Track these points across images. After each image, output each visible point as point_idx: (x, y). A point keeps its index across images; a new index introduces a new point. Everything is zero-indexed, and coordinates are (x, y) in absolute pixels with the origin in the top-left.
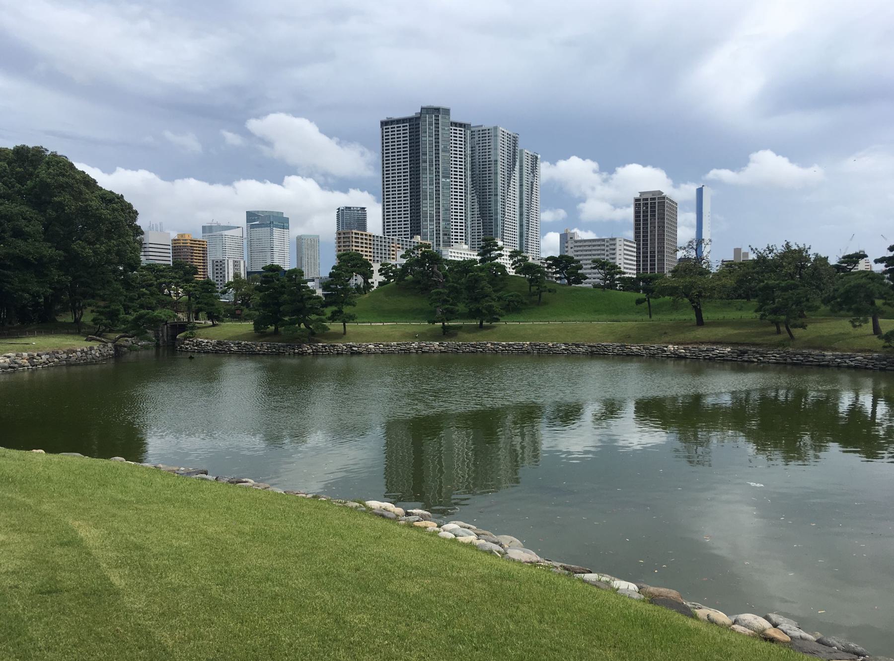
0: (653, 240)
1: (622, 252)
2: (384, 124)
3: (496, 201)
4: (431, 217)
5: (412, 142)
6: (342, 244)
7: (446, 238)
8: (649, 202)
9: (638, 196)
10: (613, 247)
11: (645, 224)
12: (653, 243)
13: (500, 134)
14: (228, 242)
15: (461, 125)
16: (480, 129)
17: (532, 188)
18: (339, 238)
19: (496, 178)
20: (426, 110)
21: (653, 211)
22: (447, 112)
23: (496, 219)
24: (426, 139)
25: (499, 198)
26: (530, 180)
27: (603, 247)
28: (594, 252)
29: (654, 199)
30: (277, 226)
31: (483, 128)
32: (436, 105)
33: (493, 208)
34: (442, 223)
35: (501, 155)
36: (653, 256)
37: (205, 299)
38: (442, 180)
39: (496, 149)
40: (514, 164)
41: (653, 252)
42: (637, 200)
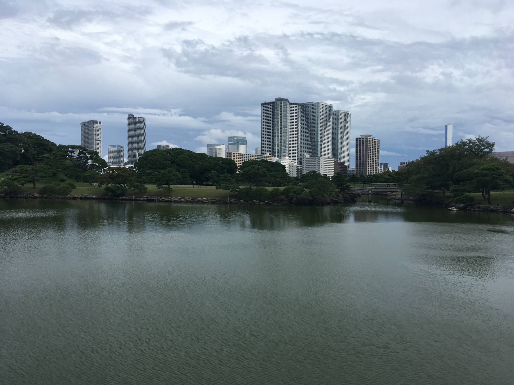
0: (363, 156)
1: (323, 168)
2: (263, 104)
3: (317, 136)
11: (360, 149)
13: (320, 105)
15: (296, 104)
19: (318, 126)
21: (363, 144)
22: (286, 100)
23: (317, 144)
25: (319, 135)
30: (241, 144)
38: (283, 129)
39: (318, 113)
40: (329, 119)
42: (357, 139)
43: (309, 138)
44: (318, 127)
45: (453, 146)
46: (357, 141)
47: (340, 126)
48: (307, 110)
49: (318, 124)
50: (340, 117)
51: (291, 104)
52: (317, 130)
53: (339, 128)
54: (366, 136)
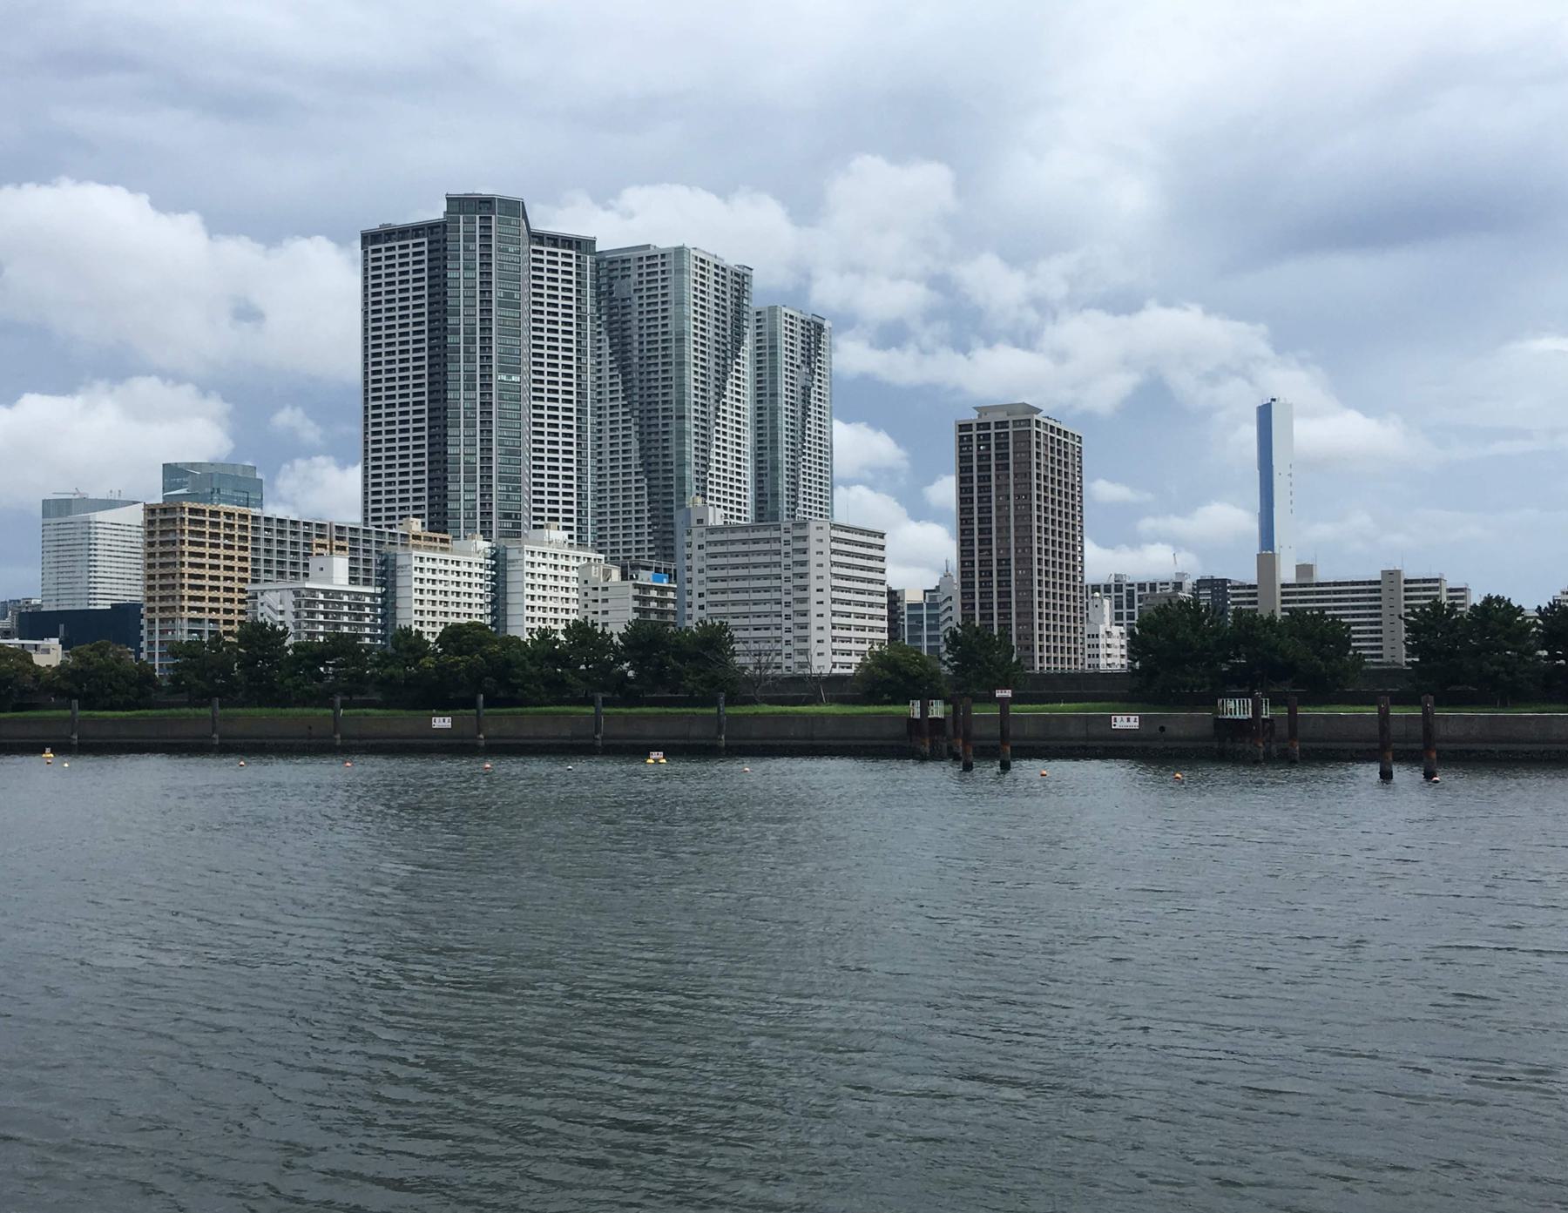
1: (827, 558)
2: (369, 238)
3: (682, 433)
4: (470, 470)
5: (439, 280)
6: (157, 538)
7: (508, 524)
8: (993, 431)
9: (972, 416)
10: (800, 545)
11: (984, 489)
12: (1003, 539)
13: (691, 265)
14: (103, 539)
15: (568, 242)
16: (644, 253)
17: (806, 408)
18: (151, 523)
20: (458, 204)
22: (515, 209)
23: (682, 479)
24: (460, 275)
25: (690, 425)
26: (800, 382)
27: (775, 546)
28: (755, 559)
29: (1004, 424)
31: (651, 252)
32: (485, 191)
33: (673, 451)
34: (497, 488)
35: (694, 321)
36: (1004, 573)
37: (1302, 759)
40: (738, 342)
41: (1004, 562)
42: (964, 427)
43: (635, 445)
44: (681, 385)
45: (581, 632)
46: (964, 442)
47: (782, 389)
48: (625, 294)
49: (681, 364)
50: (782, 343)
51: (540, 238)
52: (681, 402)
53: (782, 401)
54: (1010, 408)
